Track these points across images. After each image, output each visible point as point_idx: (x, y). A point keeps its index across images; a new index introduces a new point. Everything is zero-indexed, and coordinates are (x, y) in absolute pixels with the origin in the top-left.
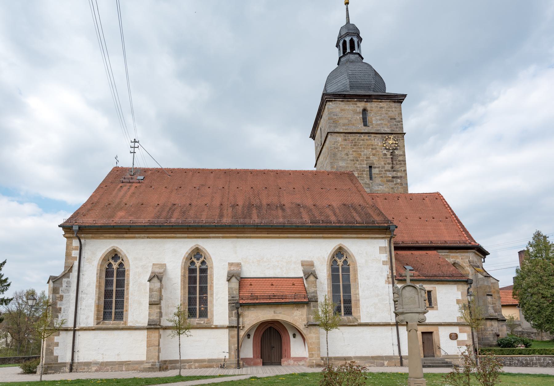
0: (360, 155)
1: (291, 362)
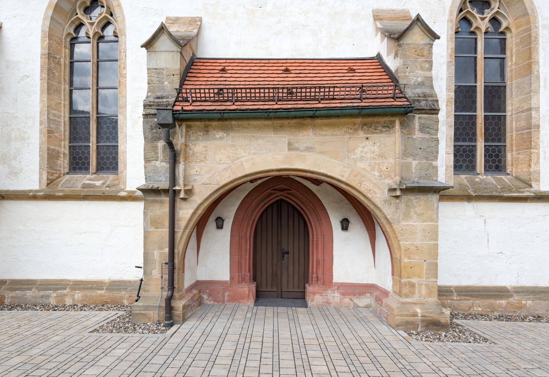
1: (335, 297)
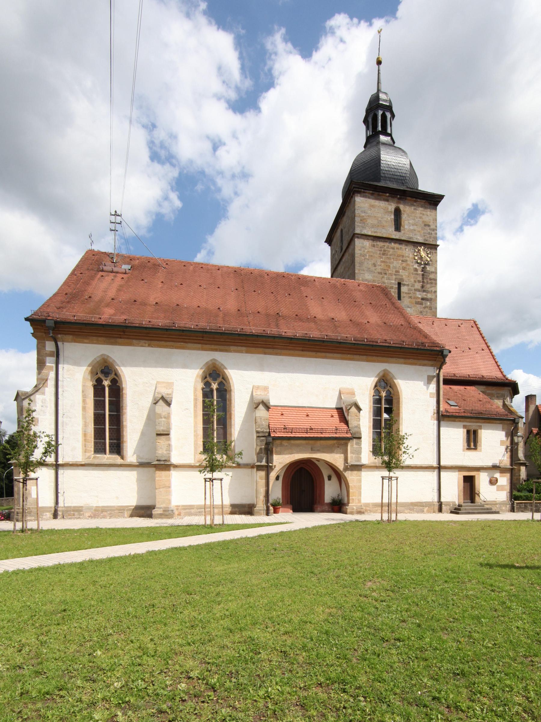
0: (389, 267)
